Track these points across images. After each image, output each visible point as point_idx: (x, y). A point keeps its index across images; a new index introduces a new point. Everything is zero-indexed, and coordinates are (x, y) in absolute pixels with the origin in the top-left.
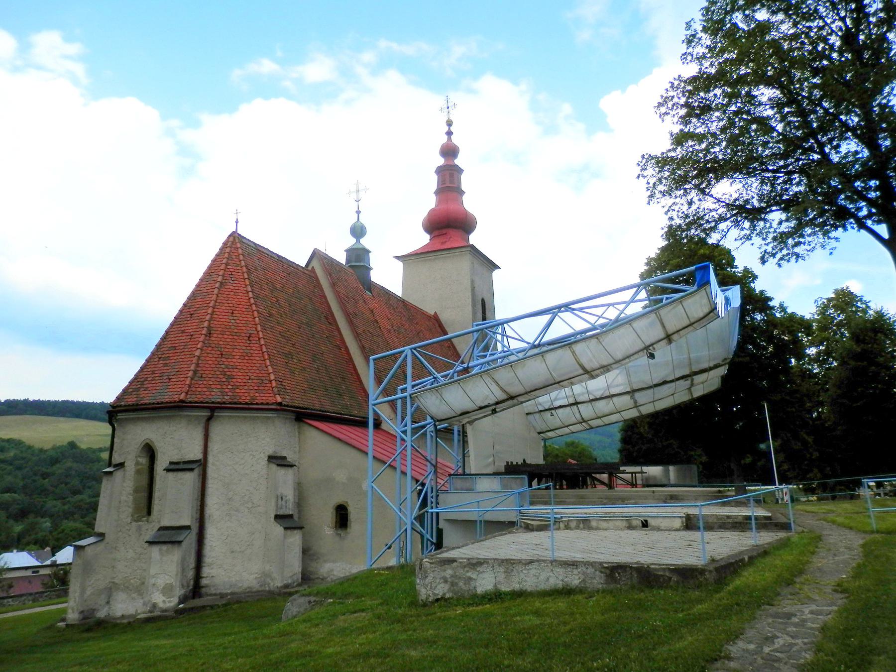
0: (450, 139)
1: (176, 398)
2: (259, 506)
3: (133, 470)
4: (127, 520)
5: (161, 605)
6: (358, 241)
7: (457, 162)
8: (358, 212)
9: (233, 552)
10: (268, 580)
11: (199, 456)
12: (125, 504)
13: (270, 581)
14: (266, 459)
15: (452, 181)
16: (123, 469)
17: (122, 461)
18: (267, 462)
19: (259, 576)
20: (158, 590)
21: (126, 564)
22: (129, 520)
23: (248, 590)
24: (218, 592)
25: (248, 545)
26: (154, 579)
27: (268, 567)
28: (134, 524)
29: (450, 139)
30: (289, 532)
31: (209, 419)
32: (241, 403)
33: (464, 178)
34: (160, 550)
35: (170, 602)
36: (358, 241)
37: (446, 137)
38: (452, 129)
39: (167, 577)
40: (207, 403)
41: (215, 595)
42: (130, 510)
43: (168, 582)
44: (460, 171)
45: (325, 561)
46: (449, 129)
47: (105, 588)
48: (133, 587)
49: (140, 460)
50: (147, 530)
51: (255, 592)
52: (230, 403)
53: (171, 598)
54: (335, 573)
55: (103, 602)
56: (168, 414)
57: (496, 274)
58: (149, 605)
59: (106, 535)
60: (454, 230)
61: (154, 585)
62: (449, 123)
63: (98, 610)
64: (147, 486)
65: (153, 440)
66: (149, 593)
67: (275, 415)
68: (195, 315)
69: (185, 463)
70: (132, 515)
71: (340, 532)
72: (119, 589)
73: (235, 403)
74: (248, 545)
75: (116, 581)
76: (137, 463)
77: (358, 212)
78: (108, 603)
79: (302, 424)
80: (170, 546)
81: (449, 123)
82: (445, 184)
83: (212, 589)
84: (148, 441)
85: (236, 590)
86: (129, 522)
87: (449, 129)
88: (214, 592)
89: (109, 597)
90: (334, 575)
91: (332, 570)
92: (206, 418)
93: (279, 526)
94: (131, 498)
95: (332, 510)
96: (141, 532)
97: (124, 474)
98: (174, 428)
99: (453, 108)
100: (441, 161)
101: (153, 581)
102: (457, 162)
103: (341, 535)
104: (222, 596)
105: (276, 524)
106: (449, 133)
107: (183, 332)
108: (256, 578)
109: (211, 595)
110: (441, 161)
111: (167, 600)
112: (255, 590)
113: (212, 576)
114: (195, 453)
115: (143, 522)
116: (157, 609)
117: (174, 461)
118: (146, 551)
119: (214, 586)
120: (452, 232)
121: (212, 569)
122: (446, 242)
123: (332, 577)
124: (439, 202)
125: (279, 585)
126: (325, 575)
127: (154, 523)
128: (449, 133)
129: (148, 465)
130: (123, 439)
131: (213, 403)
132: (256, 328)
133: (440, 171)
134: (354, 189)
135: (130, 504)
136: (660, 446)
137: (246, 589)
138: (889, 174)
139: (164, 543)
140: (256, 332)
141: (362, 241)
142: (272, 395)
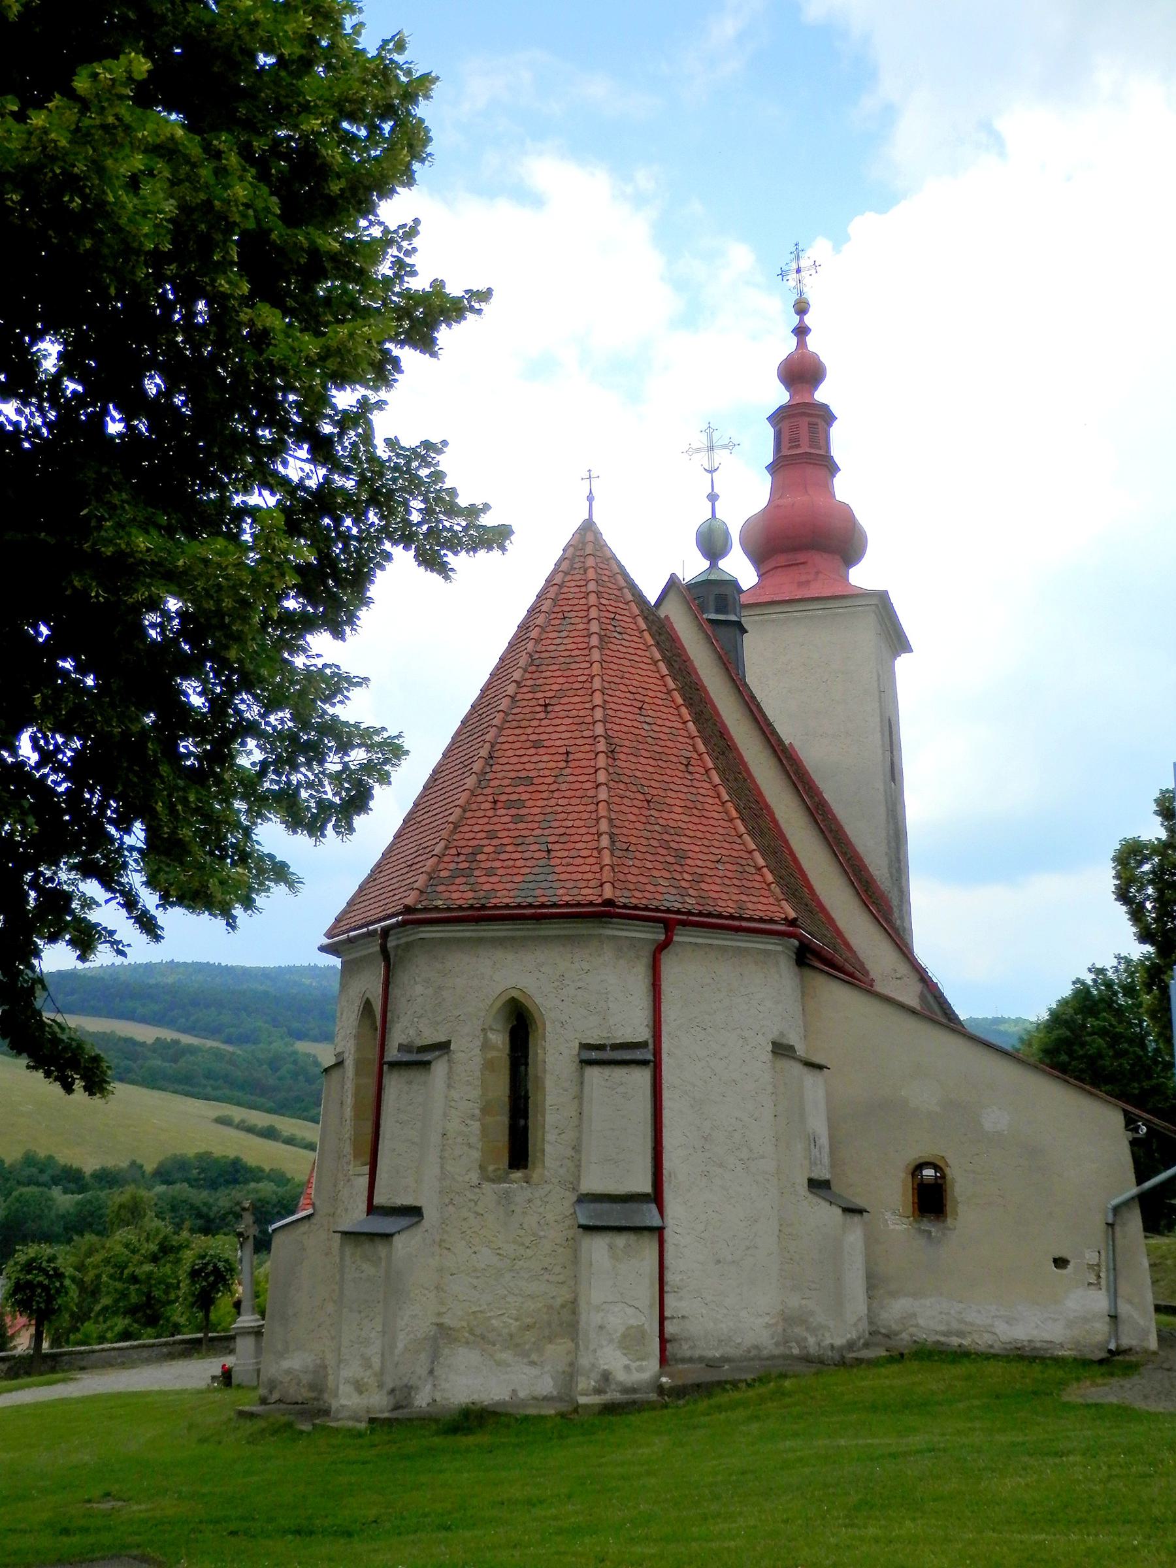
0: (802, 344)
1: (589, 894)
2: (763, 1157)
3: (478, 1060)
4: (467, 1178)
5: (621, 1376)
6: (714, 565)
7: (822, 395)
8: (713, 498)
9: (719, 1262)
10: (799, 1331)
11: (642, 1033)
12: (459, 1140)
13: (805, 1334)
14: (770, 1047)
15: (814, 442)
16: (446, 1058)
17: (443, 1039)
18: (770, 1055)
19: (773, 1321)
20: (611, 1341)
21: (475, 1282)
22: (474, 1177)
23: (754, 1353)
24: (697, 1353)
25: (748, 1248)
26: (601, 1314)
27: (794, 1301)
28: (488, 1187)
29: (802, 344)
30: (849, 1216)
31: (662, 947)
32: (720, 916)
33: (837, 433)
34: (611, 1247)
35: (640, 1369)
36: (714, 565)
37: (793, 341)
38: (808, 320)
39: (630, 1311)
40: (657, 910)
41: (691, 1360)
42: (476, 1155)
43: (633, 1322)
44: (825, 416)
45: (893, 1295)
46: (801, 320)
47: (425, 1339)
48: (500, 1335)
49: (492, 1037)
50: (530, 1201)
51: (767, 1359)
52: (700, 914)
53: (642, 1359)
54: (921, 1322)
55: (422, 1371)
56: (562, 932)
57: (903, 663)
58: (592, 1375)
59: (425, 1211)
60: (825, 556)
61: (601, 1327)
62: (801, 308)
63: (417, 1388)
64: (507, 1099)
65: (531, 991)
66: (592, 1347)
67: (780, 948)
68: (557, 708)
69: (616, 1047)
70: (481, 1167)
71: (926, 1225)
72: (456, 1340)
73: (709, 915)
74: (748, 1248)
75: (446, 1320)
76: (486, 1046)
77: (713, 498)
78: (431, 1372)
79: (809, 974)
80: (631, 1238)
81: (801, 308)
82: (798, 446)
83: (685, 1347)
84: (515, 994)
85: (730, 1351)
86: (475, 1181)
87: (801, 320)
88: (688, 1354)
89: (435, 1357)
90: (917, 1326)
91: (914, 1315)
92: (653, 947)
93: (827, 1205)
94: (476, 1126)
95: (902, 1175)
96: (513, 1207)
97: (451, 1068)
98: (585, 966)
99: (813, 272)
100: (780, 396)
101: (597, 1319)
102: (822, 395)
103: (930, 1232)
104: (712, 1364)
105: (815, 1199)
106: (801, 332)
107: (537, 745)
108: (768, 1326)
109: (683, 1360)
110: (780, 396)
111: (634, 1365)
112: (765, 1353)
113: (683, 1317)
114: (636, 1029)
115: (512, 1182)
116: (613, 1387)
117: (592, 1042)
118: (529, 1252)
119: (686, 1339)
120: (819, 560)
121: (681, 1299)
122: (808, 582)
123: (912, 1330)
124: (777, 490)
125: (839, 1342)
126: (894, 1327)
127: (547, 1188)
128: (801, 332)
129: (507, 1051)
130: (440, 988)
131: (668, 911)
132: (693, 746)
133: (781, 418)
134: (701, 440)
135: (473, 1140)
136: (1136, 1092)
137: (749, 1352)
138: (245, 522)
139: (620, 1229)
140: (695, 756)
141: (722, 564)
142: (772, 900)
